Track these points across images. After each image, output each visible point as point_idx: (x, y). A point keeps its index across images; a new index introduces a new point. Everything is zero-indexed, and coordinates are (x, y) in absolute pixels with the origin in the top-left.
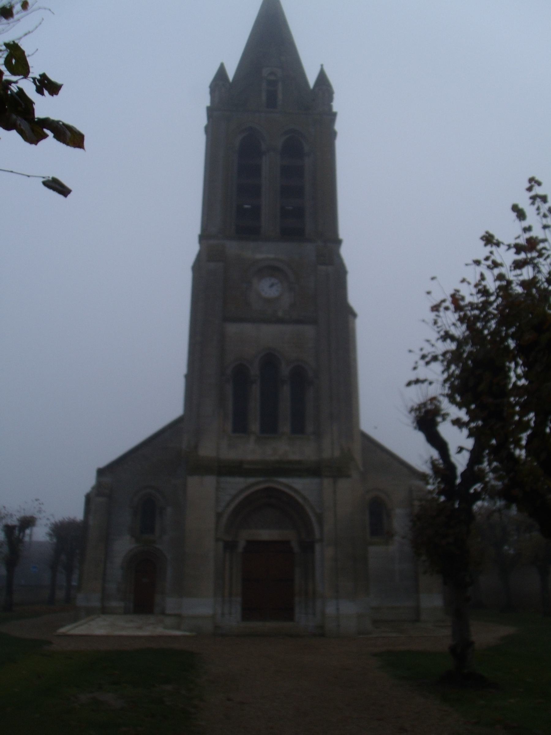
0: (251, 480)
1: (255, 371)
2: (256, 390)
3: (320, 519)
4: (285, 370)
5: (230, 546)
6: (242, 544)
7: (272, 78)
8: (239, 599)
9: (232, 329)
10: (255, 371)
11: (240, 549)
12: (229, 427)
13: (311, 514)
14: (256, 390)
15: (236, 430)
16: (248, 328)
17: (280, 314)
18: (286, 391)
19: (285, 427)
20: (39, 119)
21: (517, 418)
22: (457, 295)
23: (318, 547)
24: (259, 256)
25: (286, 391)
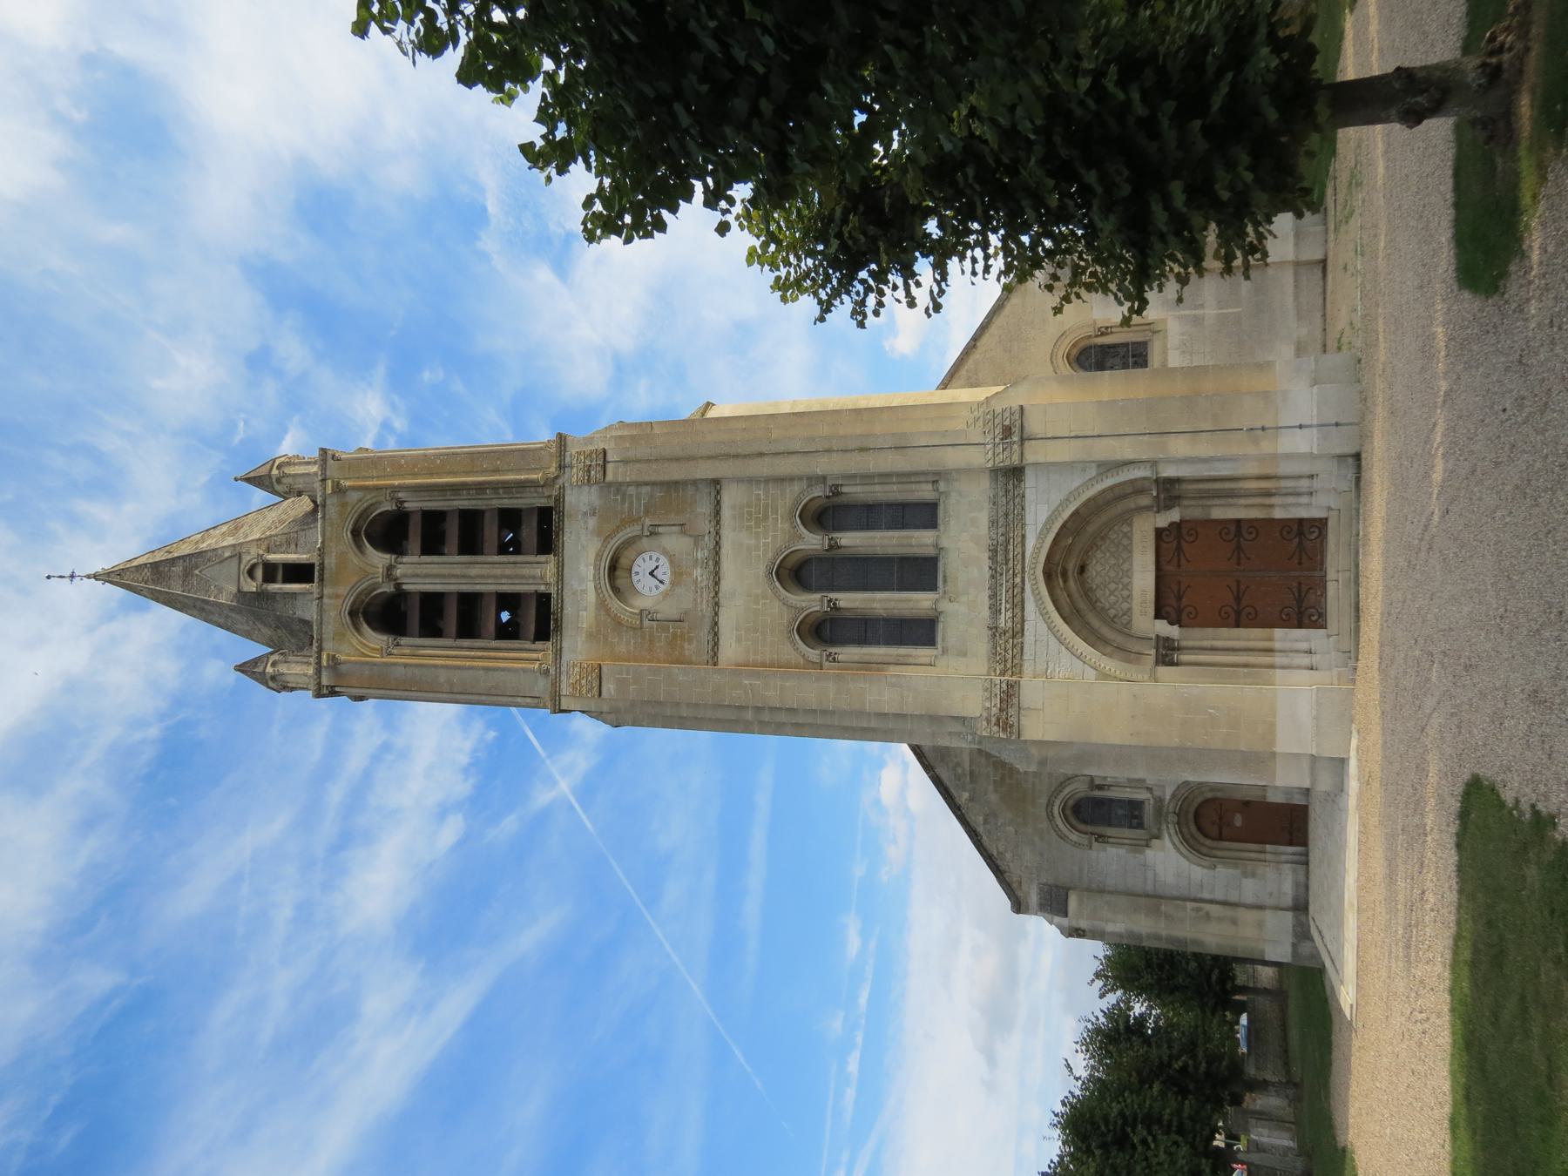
0: (1030, 606)
1: (812, 602)
2: (849, 600)
3: (1108, 467)
4: (813, 542)
5: (1167, 654)
6: (1164, 628)
7: (259, 573)
8: (1279, 633)
9: (730, 650)
10: (812, 602)
11: (1173, 631)
12: (923, 653)
13: (1099, 487)
14: (849, 600)
15: (930, 641)
16: (729, 619)
17: (311, 671)
18: (852, 540)
19: (918, 541)
20: (947, 264)
21: (903, 127)
22: (709, 551)
23: (1169, 472)
24: (591, 596)
25: (852, 540)
